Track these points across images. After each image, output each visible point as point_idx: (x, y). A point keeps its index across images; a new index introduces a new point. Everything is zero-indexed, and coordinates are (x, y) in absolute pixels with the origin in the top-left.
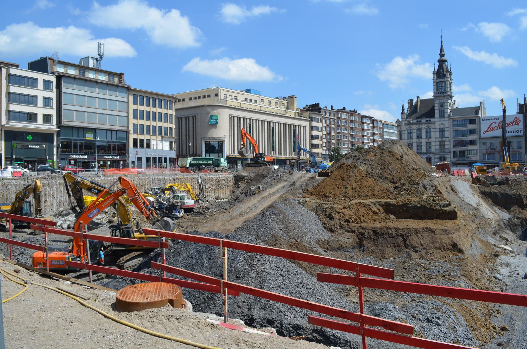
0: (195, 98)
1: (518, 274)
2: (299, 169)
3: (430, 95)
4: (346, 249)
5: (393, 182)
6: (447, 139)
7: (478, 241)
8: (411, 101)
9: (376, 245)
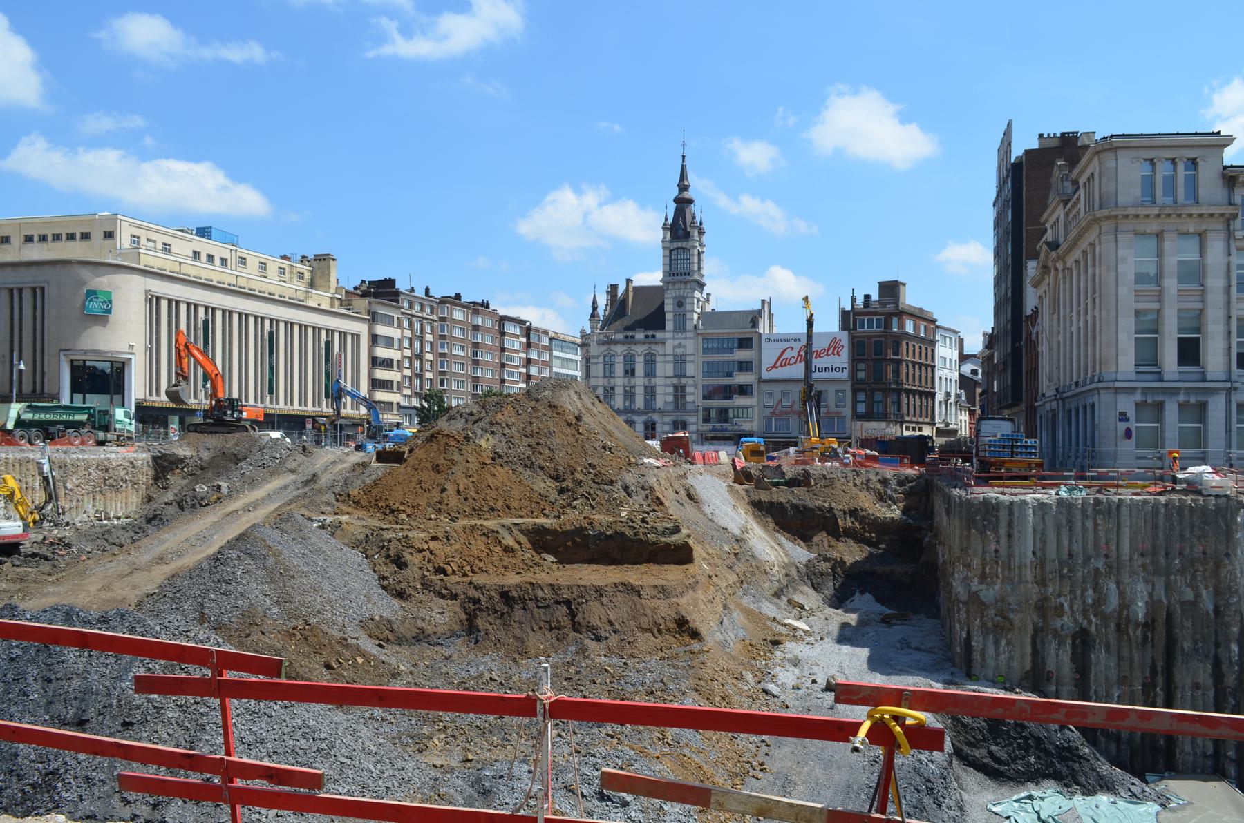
0: (43, 238)
1: (814, 682)
2: (335, 441)
3: (652, 277)
4: (434, 639)
5: (556, 478)
6: (690, 381)
7: (738, 611)
8: (614, 288)
9: (507, 626)
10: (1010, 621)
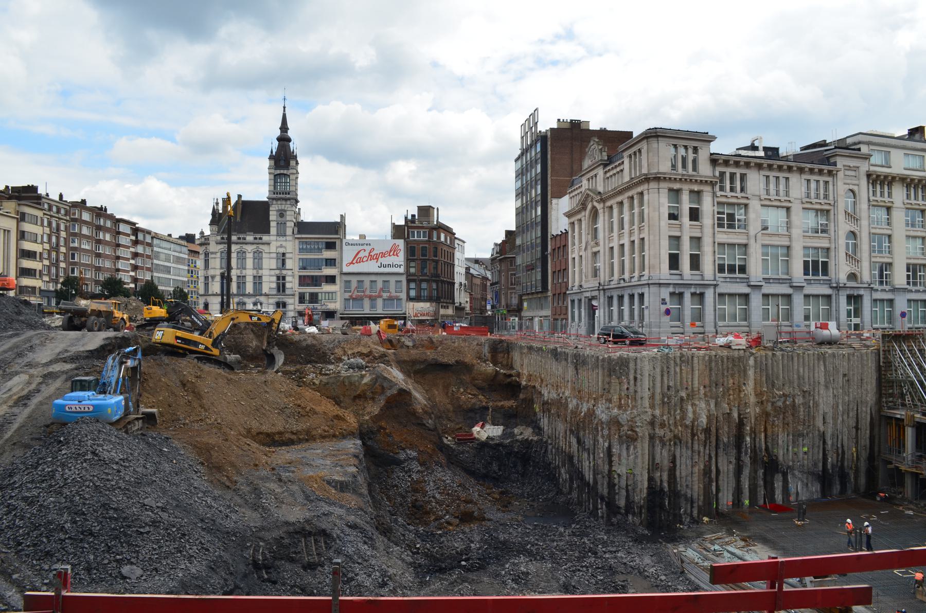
6: (290, 273)
10: (636, 432)
